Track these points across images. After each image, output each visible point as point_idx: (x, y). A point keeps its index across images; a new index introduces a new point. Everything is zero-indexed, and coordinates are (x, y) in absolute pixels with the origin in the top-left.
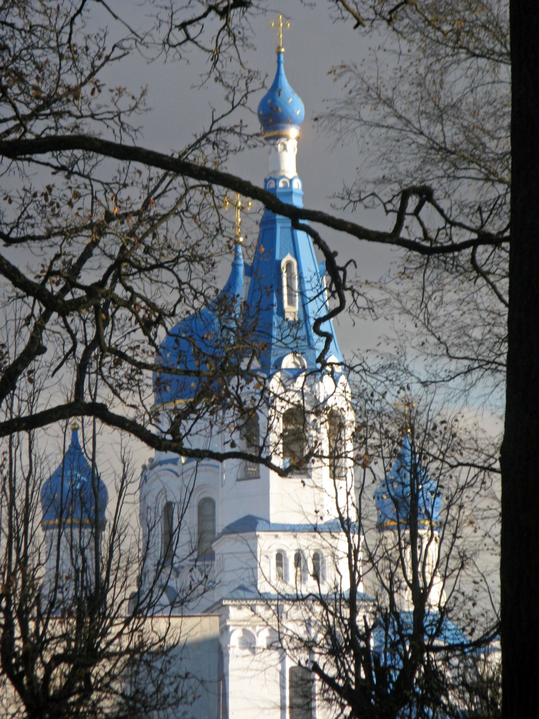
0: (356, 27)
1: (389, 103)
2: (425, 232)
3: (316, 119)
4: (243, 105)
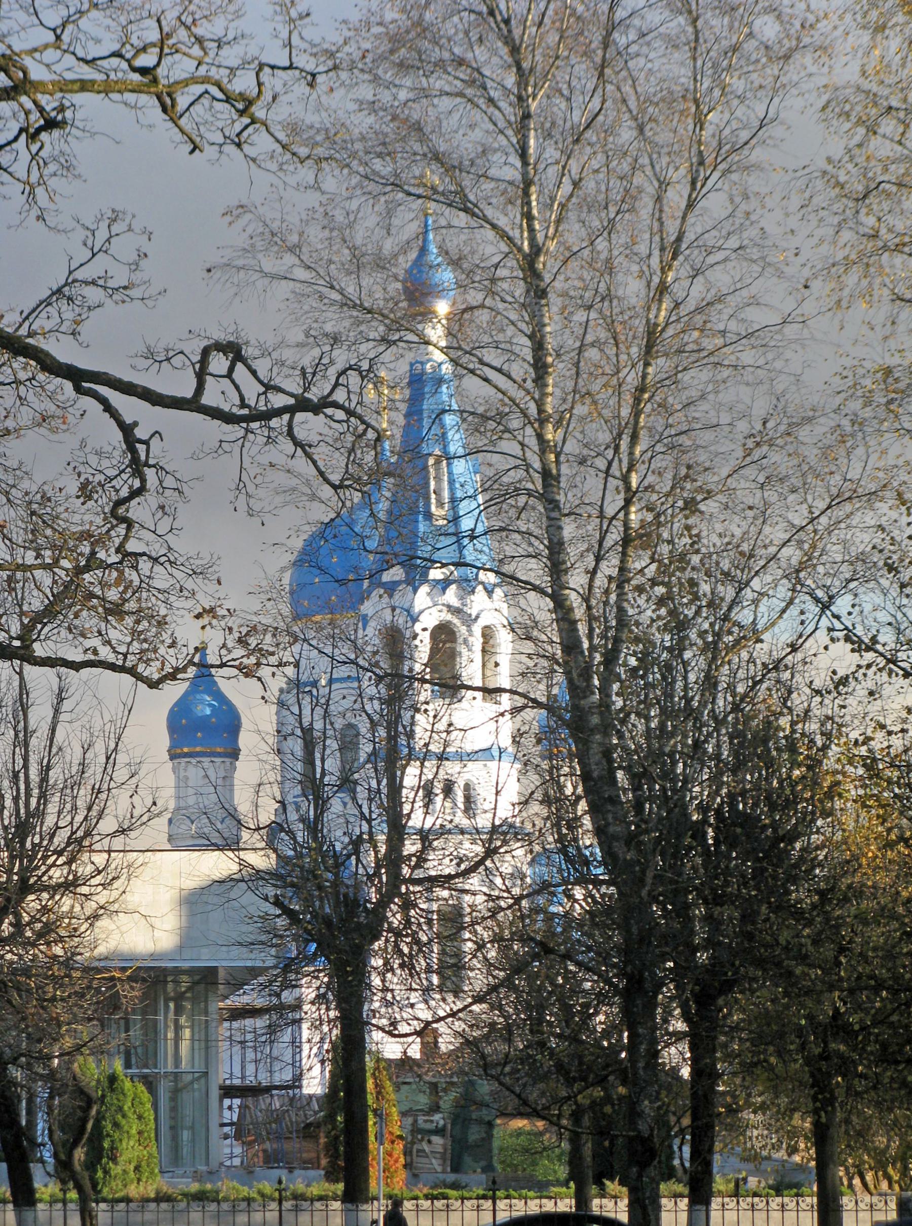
0: (192, 152)
1: (294, 249)
2: (242, 399)
3: (209, 270)
4: (106, 252)
